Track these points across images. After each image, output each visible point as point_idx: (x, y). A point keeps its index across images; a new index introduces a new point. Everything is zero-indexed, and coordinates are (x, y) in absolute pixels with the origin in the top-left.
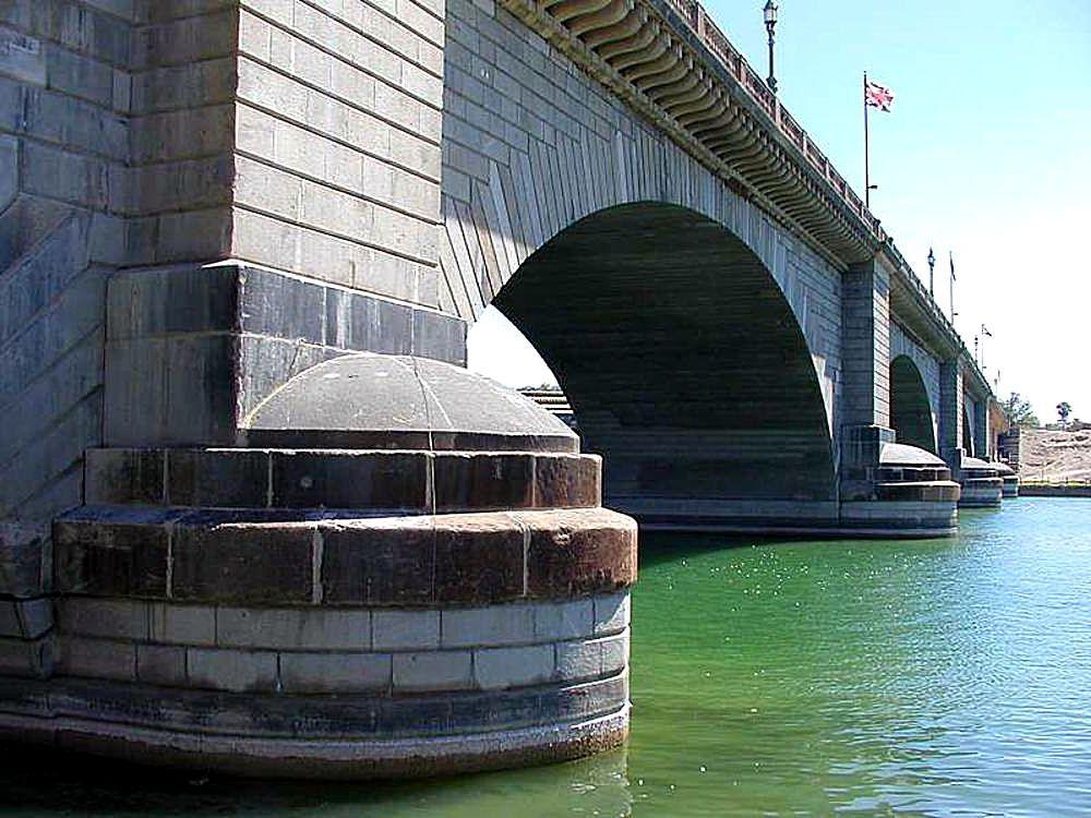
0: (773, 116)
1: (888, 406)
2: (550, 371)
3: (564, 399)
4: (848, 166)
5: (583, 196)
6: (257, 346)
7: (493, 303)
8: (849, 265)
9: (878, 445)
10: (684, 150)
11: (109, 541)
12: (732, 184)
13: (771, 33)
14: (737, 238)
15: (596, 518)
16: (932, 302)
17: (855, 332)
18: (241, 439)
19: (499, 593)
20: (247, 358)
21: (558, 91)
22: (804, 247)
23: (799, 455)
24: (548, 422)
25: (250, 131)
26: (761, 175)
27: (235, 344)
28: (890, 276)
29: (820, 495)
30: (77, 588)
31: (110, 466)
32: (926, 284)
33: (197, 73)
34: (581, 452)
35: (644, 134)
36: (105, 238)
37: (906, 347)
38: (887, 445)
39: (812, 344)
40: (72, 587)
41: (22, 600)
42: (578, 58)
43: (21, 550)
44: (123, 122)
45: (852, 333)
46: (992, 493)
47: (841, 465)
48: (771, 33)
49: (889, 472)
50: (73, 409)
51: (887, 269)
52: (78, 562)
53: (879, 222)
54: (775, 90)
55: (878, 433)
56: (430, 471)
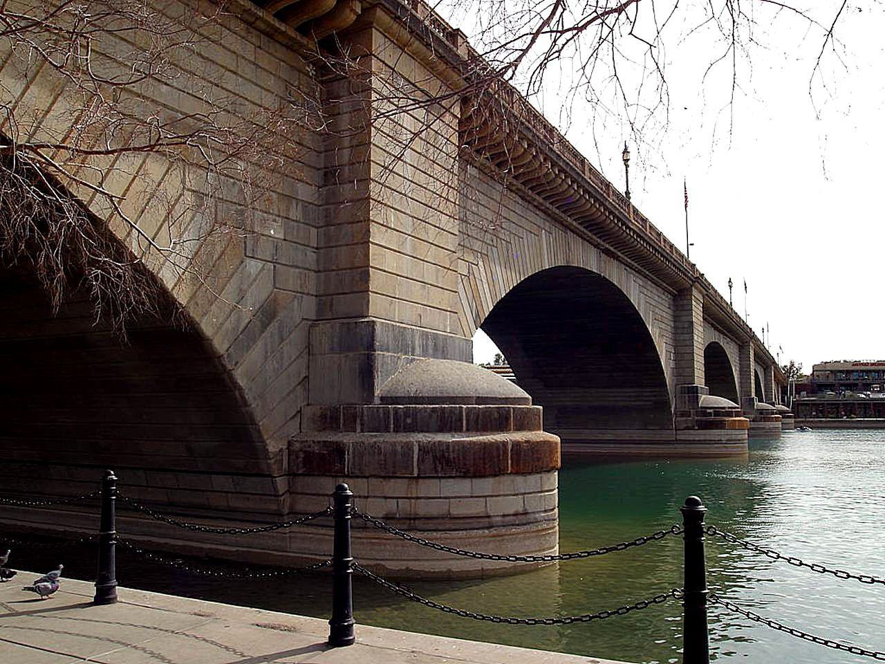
0: (629, 213)
1: (703, 373)
2: (488, 337)
3: (513, 374)
4: (675, 235)
5: (525, 267)
6: (382, 357)
7: (481, 327)
8: (677, 291)
9: (698, 396)
10: (579, 236)
11: (316, 449)
12: (607, 252)
13: (627, 166)
14: (610, 281)
15: (541, 435)
16: (732, 309)
17: (682, 331)
18: (377, 401)
19: (498, 472)
20: (378, 363)
21: (512, 212)
22: (649, 282)
23: (650, 403)
24: (507, 386)
25: (377, 257)
26: (622, 244)
27: (373, 357)
28: (703, 296)
29: (664, 426)
30: (300, 472)
31: (314, 415)
32: (727, 298)
33: (350, 230)
34: (533, 405)
35: (557, 229)
36: (309, 307)
37: (715, 337)
38: (704, 396)
39: (655, 338)
40: (298, 471)
41: (276, 477)
42: (520, 194)
43: (276, 454)
44: (315, 252)
45: (679, 331)
46: (776, 424)
47: (676, 408)
48: (627, 166)
49: (704, 411)
50: (294, 389)
51: (701, 292)
52: (301, 459)
53: (695, 265)
54: (630, 198)
55: (697, 390)
56: (392, 412)
